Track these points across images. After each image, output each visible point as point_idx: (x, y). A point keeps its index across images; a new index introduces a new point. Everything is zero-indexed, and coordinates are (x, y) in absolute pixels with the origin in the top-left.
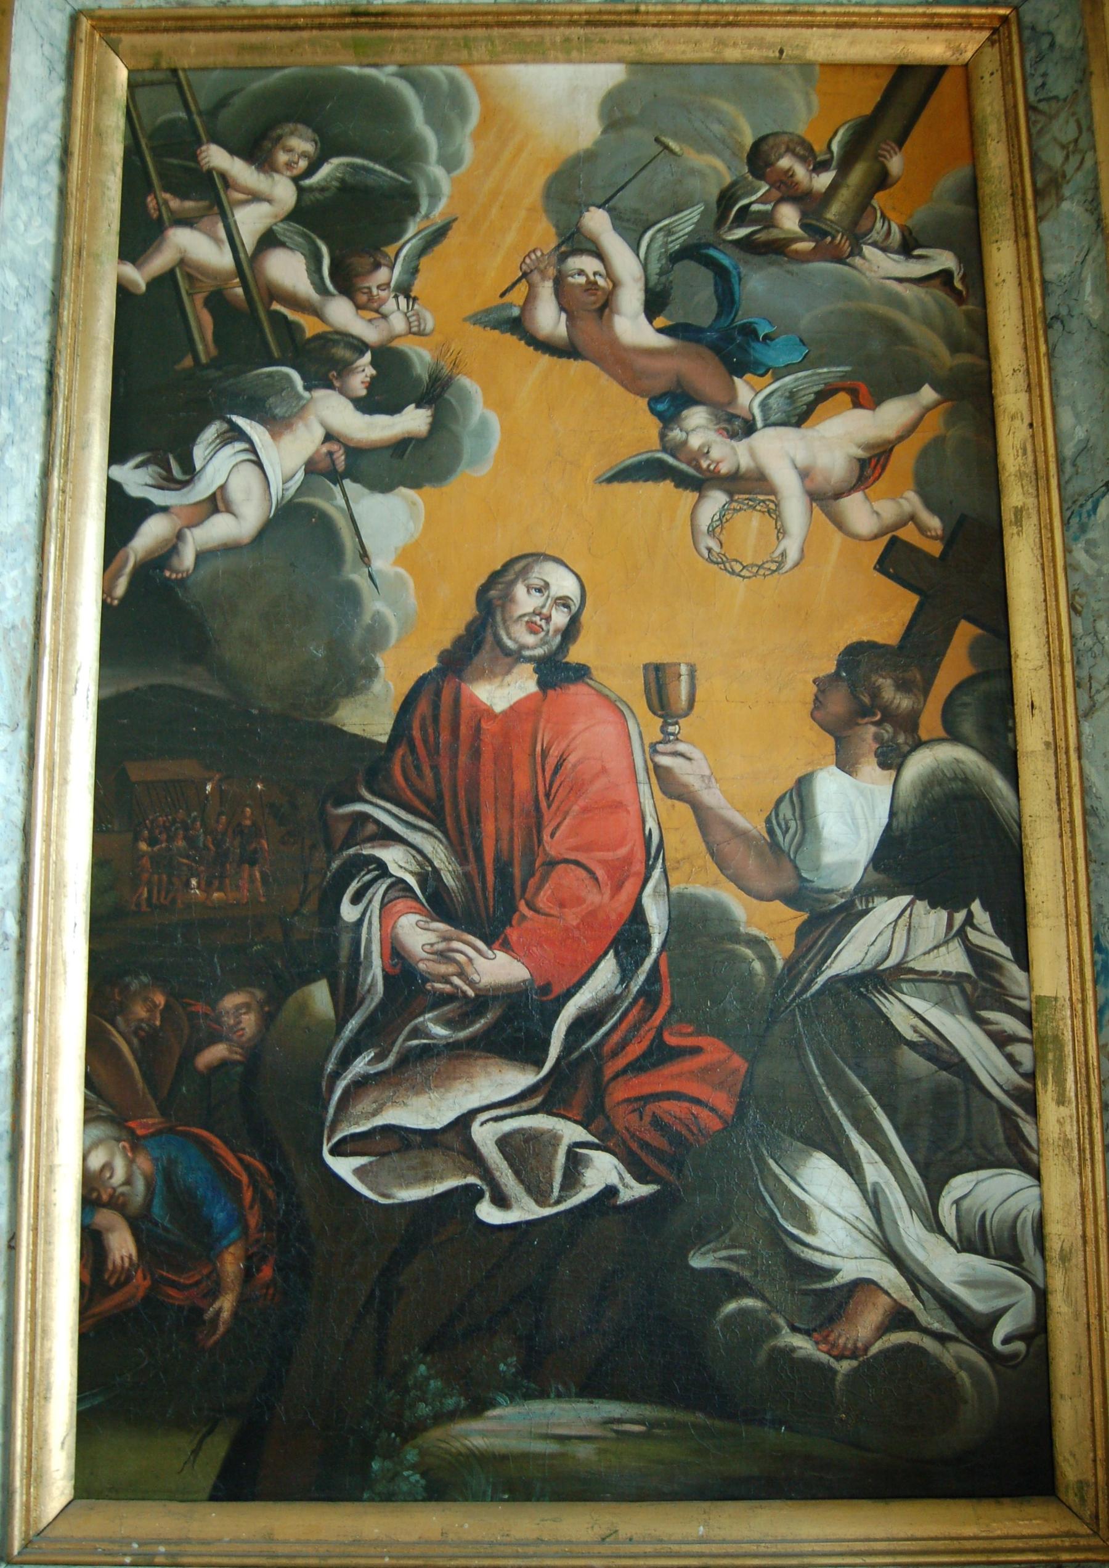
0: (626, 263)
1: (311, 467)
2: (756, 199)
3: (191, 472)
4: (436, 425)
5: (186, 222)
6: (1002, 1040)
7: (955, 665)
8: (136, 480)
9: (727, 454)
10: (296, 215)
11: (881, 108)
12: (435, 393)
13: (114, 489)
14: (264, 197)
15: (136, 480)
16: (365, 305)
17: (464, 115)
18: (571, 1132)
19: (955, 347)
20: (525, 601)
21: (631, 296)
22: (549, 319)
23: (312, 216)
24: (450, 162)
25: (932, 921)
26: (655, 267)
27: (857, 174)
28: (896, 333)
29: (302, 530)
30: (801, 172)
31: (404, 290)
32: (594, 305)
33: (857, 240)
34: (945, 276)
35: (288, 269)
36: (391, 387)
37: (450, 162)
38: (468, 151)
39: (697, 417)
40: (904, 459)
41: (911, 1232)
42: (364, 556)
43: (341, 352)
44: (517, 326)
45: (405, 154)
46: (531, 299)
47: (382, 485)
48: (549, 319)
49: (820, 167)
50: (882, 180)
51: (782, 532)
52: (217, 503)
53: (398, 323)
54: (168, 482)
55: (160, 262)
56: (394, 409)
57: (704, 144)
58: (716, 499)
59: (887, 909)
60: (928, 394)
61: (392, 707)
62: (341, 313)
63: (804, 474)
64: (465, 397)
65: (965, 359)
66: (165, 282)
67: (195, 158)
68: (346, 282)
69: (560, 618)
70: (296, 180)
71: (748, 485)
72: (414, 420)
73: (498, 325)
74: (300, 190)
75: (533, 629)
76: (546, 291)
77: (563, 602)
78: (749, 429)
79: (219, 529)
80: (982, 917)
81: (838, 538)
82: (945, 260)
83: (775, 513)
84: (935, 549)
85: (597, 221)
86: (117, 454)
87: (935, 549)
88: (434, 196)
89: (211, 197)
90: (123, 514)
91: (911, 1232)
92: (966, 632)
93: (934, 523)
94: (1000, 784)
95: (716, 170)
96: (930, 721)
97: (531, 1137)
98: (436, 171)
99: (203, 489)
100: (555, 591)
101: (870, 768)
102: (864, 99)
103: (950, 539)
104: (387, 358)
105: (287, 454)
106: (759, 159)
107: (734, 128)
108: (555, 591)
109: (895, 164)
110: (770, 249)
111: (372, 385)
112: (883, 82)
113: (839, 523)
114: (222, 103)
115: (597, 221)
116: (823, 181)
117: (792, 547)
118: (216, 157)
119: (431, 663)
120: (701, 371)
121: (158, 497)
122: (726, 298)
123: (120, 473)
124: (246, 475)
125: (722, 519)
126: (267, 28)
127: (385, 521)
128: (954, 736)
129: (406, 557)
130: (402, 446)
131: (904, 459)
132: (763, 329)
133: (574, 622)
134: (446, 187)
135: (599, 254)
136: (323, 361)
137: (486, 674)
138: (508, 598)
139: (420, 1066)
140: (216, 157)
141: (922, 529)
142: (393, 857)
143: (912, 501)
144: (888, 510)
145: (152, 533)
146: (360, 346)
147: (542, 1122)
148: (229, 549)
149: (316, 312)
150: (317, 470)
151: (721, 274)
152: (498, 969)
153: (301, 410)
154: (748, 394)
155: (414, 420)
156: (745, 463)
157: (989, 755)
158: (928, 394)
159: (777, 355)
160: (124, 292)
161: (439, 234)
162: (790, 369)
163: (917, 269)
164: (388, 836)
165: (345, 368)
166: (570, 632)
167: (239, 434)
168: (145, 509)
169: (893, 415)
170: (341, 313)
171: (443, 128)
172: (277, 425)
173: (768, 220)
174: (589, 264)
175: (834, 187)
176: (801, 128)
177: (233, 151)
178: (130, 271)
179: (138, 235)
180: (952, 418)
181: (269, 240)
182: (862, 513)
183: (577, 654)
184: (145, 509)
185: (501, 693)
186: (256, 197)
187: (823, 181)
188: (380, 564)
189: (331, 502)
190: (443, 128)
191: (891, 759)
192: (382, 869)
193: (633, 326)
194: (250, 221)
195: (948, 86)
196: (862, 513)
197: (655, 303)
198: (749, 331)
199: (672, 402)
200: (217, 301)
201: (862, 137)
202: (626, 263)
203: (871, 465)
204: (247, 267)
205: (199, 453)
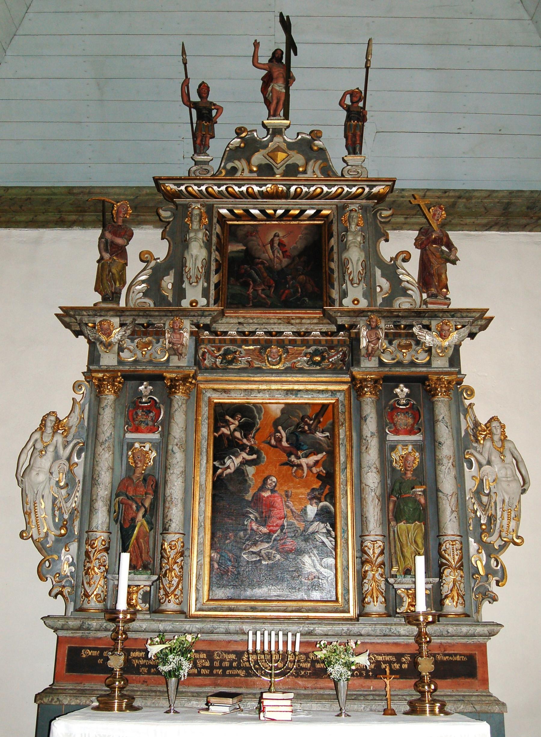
0: (284, 434)
1: (241, 462)
2: (302, 425)
3: (225, 463)
4: (258, 457)
5: (224, 427)
6: (331, 541)
7: (326, 491)
8: (217, 464)
9: (296, 461)
10: (238, 426)
11: (320, 411)
12: (257, 452)
13: (214, 465)
14: (234, 424)
15: (217, 464)
16: (248, 440)
17: (262, 412)
18: (274, 552)
19: (328, 446)
20: (269, 482)
21: (284, 439)
22: (273, 442)
23: (241, 427)
24: (260, 419)
25: (322, 525)
26: (288, 434)
27: (316, 421)
28: (321, 445)
29: (240, 472)
30: (308, 421)
31: (253, 438)
32: (279, 440)
33: (316, 431)
34: (328, 436)
35: (238, 434)
36: (252, 451)
37: (260, 419)
38: (262, 417)
39: (293, 456)
40: (321, 462)
41: (318, 567)
42: (248, 475)
43: (245, 447)
44: (269, 443)
45: (254, 418)
46: (271, 439)
47: (250, 466)
48: (273, 442)
49: (311, 420)
50: (319, 422)
51: (304, 473)
52: (228, 467)
53: (253, 442)
54: (221, 464)
55: (220, 433)
56: (252, 455)
57: (295, 417)
58: (295, 468)
59: (316, 523)
60: (324, 453)
61: (251, 495)
62: (245, 441)
63: (307, 464)
64: (261, 453)
65: (330, 448)
66: (220, 436)
67: (224, 418)
68: (246, 436)
69: (274, 484)
70: (239, 421)
71: (300, 466)
72: (255, 456)
73: (266, 443)
74: (239, 423)
75: (270, 486)
76: (273, 438)
77: (274, 482)
78: (300, 458)
79: (228, 471)
80: (329, 525)
81: (311, 474)
82: (328, 434)
83: (303, 470)
84: (324, 475)
85: (280, 428)
86: (214, 460)
87: (324, 475)
88: (258, 424)
89: (227, 424)
90: (215, 469)
91: (318, 567)
92: (328, 487)
93: (324, 471)
94: (332, 507)
95: (296, 420)
96: (323, 499)
97: (269, 552)
98: (258, 420)
99: (226, 465)
100: (273, 480)
101: (314, 505)
102: (318, 409)
103: (326, 473)
104: (251, 448)
105: (237, 461)
106: (303, 419)
107: (299, 414)
108: (273, 480)
109: (321, 420)
110: (304, 432)
111: (249, 451)
112: (321, 406)
113: (311, 471)
114: (228, 409)
115: (280, 428)
116: (312, 422)
117: (305, 475)
118: (228, 417)
119: (68, 331)
120: (293, 450)
121: (220, 466)
122: (297, 440)
123: (214, 463)
124: (232, 463)
125: (296, 470)
126: (235, 381)
127: (251, 470)
128: (326, 501)
129: (253, 475)
130: (253, 460)
131: (321, 462)
132: (302, 444)
133: (276, 485)
134: (259, 423)
135: (280, 433)
136: (243, 448)
137: (264, 491)
138: (267, 480)
139: (255, 544)
140: (228, 417)
141: (323, 472)
142: (251, 516)
143: (321, 468)
144: (318, 470)
145: (220, 471)
146: (248, 446)
147: (271, 551)
148: (230, 474)
149: (242, 441)
150: (242, 463)
151: (297, 436)
152: (265, 530)
153: (240, 454)
154: (300, 453)
155: (255, 456)
156: (299, 463)
157: (330, 503)
158: (324, 453)
159: (305, 447)
160: (215, 437)
161: (258, 429)
162: (306, 450)
163: (324, 435)
164: (251, 513)
165: (246, 449)
166: (275, 486)
167: (231, 458)
168: (218, 468)
169: (319, 457)
170: (245, 441)
171: (259, 413)
172: (236, 457)
173: (304, 428)
174: (279, 434)
175: (313, 423)
176: (308, 414)
177: (230, 417)
178: (215, 434)
179: (216, 429)
180: (327, 457)
181: (235, 430)
182: (315, 470)
183: (276, 489)
184: (218, 468)
185: (266, 494)
186: (233, 424)
187: (312, 422)
188: (250, 476)
189: (244, 468)
190: (259, 413)
191: (317, 504)
192: (250, 517)
193: (285, 444)
194: (232, 427)
195: (331, 406)
196: (315, 470)
197: (287, 441)
198: (300, 444)
199: (289, 455)
200: (228, 438)
201: (317, 416)
202: (284, 434)
203: (316, 463)
204: (232, 434)
205: (226, 460)
